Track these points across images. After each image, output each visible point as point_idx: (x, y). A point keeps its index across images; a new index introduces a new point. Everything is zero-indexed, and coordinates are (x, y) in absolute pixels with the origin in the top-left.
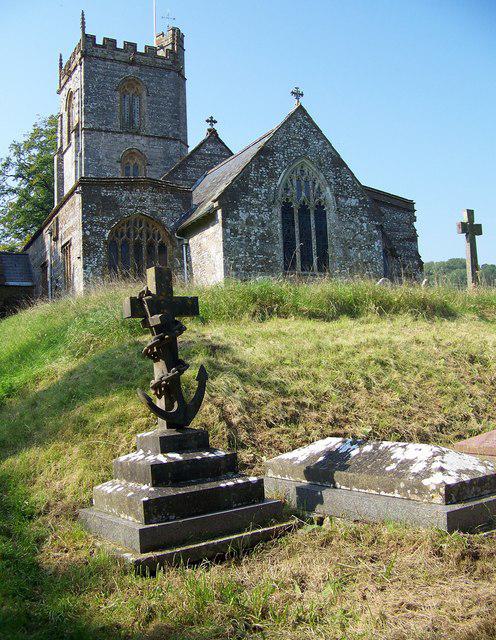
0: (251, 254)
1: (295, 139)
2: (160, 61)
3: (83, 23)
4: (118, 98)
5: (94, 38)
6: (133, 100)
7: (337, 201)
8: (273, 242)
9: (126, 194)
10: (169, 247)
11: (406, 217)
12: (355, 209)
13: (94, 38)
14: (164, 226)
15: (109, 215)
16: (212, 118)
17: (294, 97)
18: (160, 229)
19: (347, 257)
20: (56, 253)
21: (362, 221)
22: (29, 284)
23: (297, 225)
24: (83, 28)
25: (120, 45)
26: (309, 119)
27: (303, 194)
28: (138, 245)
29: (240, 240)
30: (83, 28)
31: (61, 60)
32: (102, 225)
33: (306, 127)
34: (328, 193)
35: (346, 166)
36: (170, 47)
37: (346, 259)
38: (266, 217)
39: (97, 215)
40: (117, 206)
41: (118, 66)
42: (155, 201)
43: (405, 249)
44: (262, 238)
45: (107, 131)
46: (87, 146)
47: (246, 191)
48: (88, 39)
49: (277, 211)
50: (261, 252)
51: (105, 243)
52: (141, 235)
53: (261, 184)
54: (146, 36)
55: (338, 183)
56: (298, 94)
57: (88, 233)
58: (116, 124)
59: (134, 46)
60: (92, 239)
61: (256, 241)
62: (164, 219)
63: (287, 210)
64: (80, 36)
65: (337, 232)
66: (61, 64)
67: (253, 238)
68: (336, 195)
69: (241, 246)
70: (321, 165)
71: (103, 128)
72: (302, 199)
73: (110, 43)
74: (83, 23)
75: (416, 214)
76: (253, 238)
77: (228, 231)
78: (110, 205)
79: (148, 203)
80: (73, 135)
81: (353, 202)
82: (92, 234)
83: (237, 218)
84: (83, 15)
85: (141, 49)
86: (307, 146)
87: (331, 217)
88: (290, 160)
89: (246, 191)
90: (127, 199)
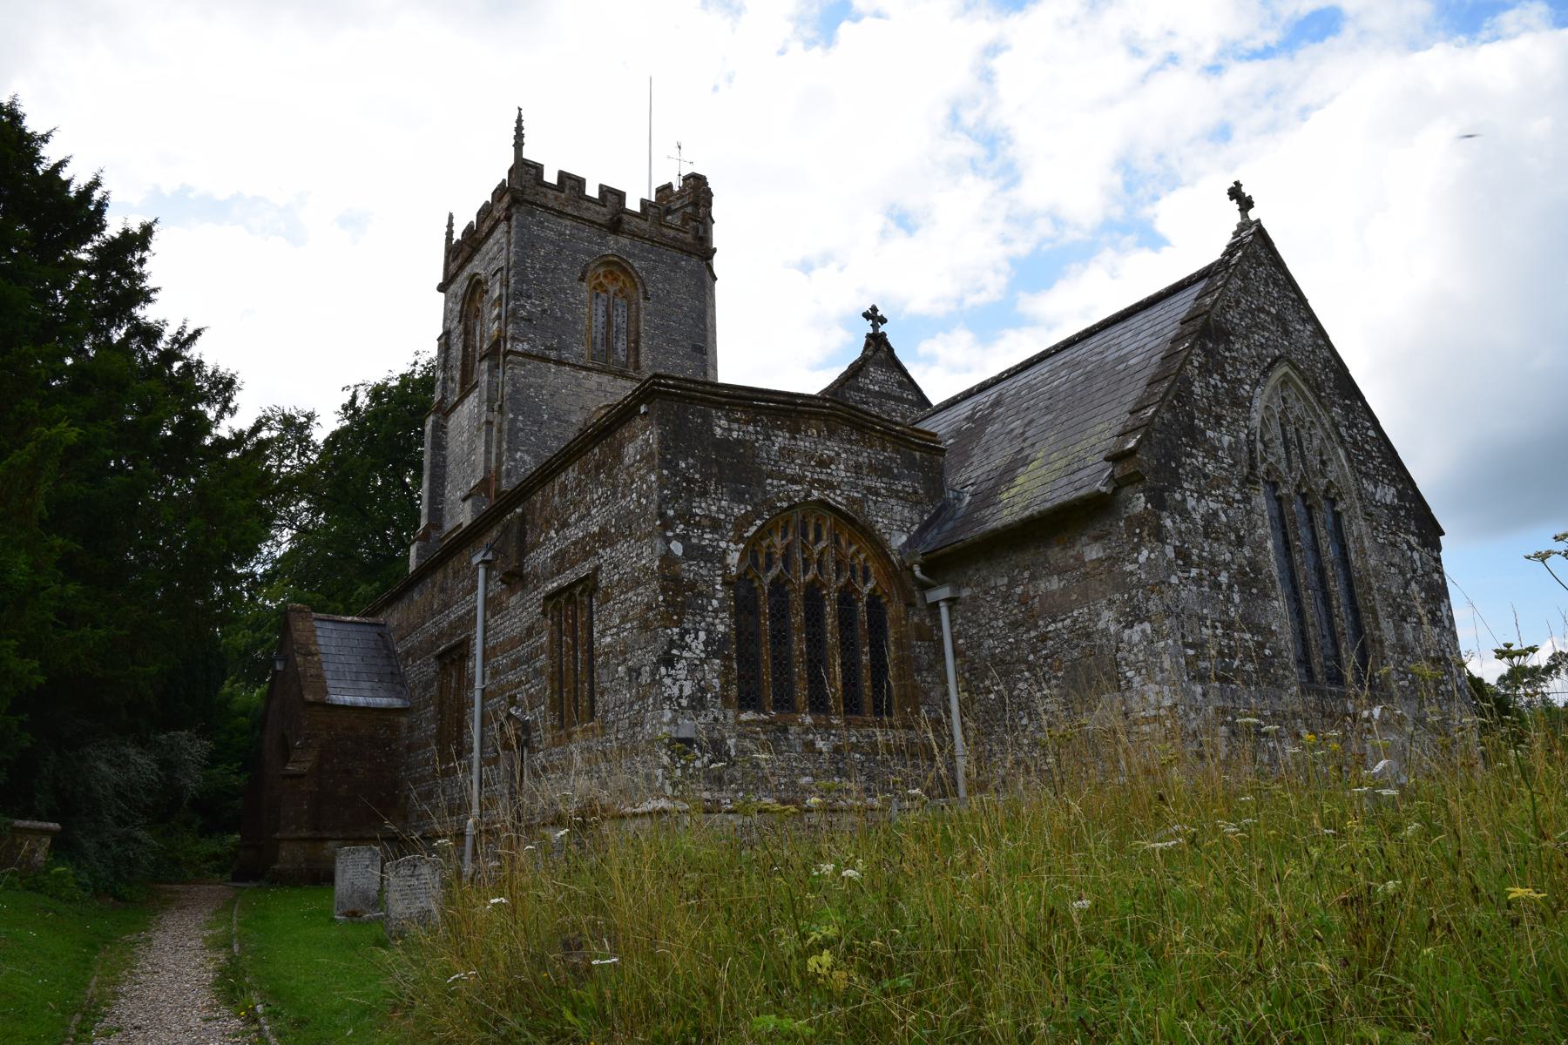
5: (538, 168)
9: (781, 439)
15: (738, 497)
16: (874, 309)
20: (853, 603)
22: (397, 703)
24: (519, 144)
30: (519, 144)
31: (450, 225)
32: (716, 526)
39: (704, 494)
41: (587, 231)
42: (858, 467)
46: (517, 391)
48: (525, 172)
57: (677, 548)
58: (579, 350)
59: (621, 196)
60: (690, 570)
64: (510, 162)
66: (450, 233)
71: (553, 354)
73: (571, 183)
79: (840, 472)
82: (693, 552)
84: (519, 121)
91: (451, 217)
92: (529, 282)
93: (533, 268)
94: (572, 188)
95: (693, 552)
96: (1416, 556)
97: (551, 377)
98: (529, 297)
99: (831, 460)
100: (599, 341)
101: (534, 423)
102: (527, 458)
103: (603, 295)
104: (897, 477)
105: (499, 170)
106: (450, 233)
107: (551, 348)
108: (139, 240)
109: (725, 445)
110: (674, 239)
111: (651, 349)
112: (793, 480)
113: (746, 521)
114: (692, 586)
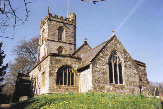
15: (57, 64)
21: (132, 69)
33: (116, 41)
34: (122, 60)
55: (125, 58)
57: (51, 69)
60: (52, 71)
87: (123, 68)
96: (133, 70)
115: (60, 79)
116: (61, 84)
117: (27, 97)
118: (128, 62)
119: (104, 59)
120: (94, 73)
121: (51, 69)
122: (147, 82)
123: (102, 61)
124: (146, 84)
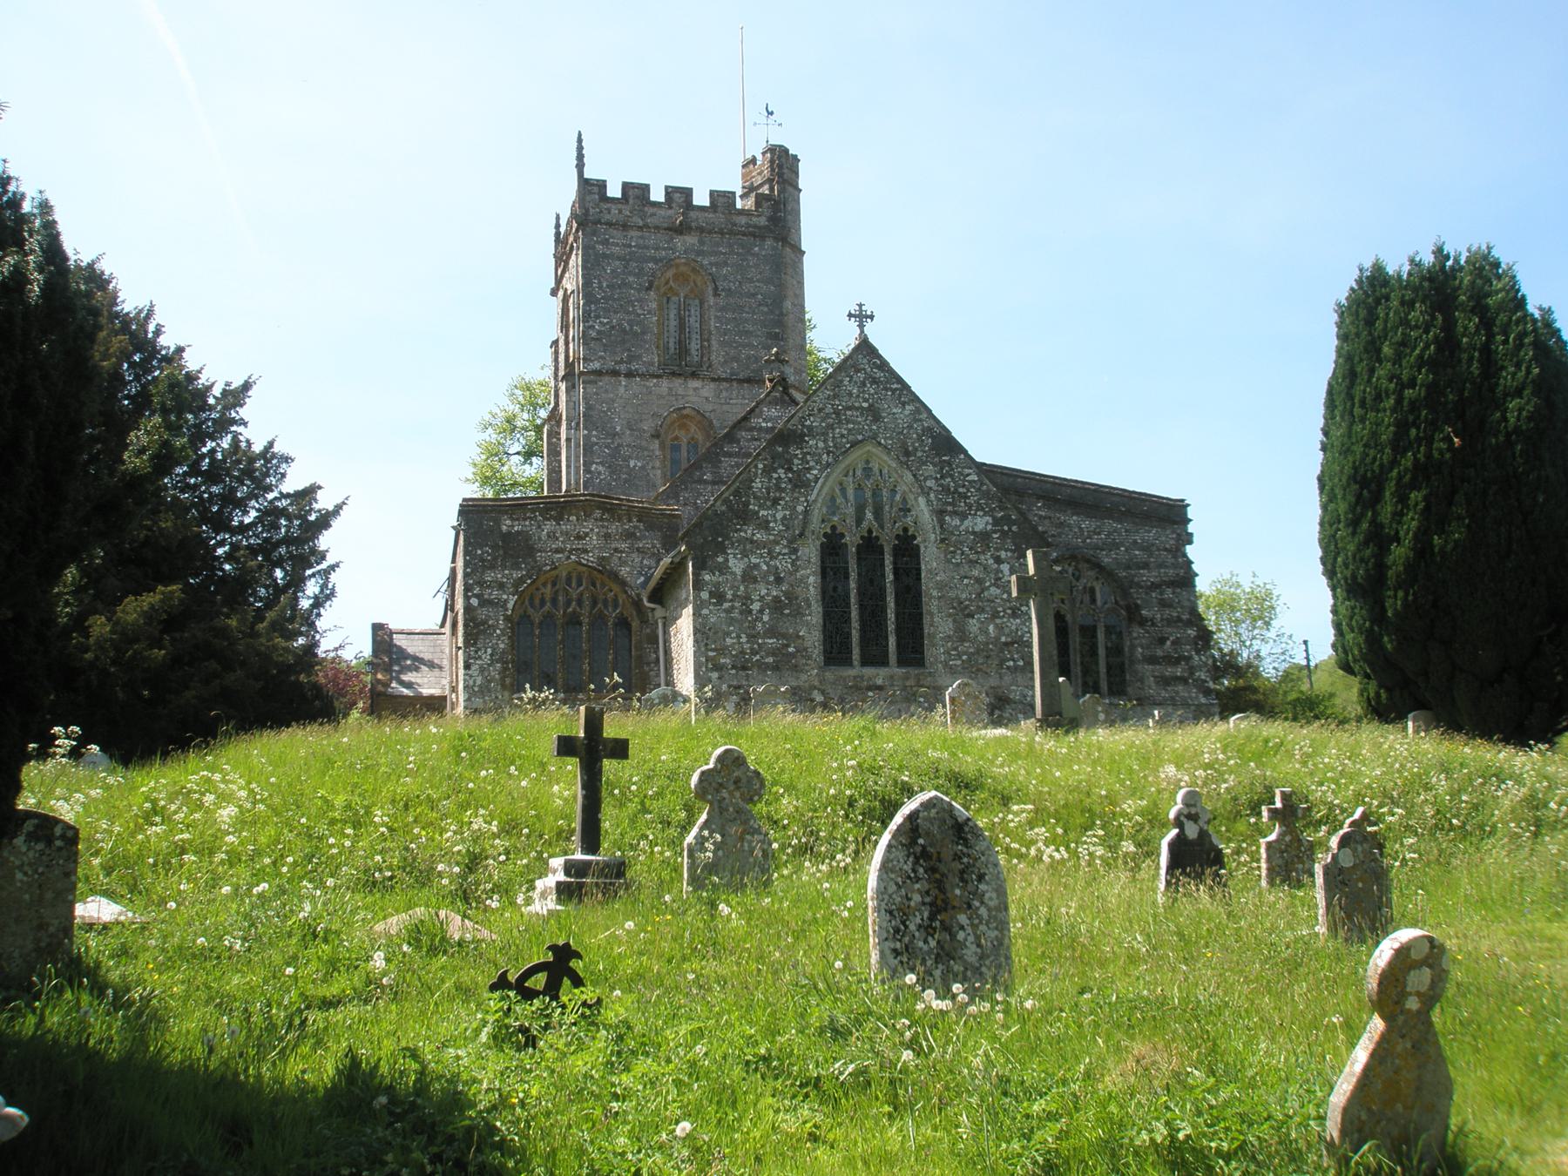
0: (752, 637)
1: (849, 408)
2: (743, 220)
3: (580, 157)
4: (654, 305)
5: (602, 185)
6: (687, 307)
7: (942, 523)
8: (798, 613)
9: (549, 526)
10: (635, 624)
11: (1168, 537)
12: (984, 536)
13: (602, 185)
14: (623, 584)
15: (516, 567)
17: (854, 324)
18: (616, 588)
19: (962, 635)
21: (998, 560)
23: (853, 575)
24: (580, 166)
25: (657, 195)
26: (884, 365)
27: (869, 515)
28: (574, 621)
29: (728, 611)
30: (580, 166)
32: (501, 586)
33: (875, 381)
34: (923, 510)
35: (965, 452)
36: (765, 190)
37: (962, 640)
38: (784, 564)
39: (492, 567)
40: (530, 551)
41: (652, 239)
42: (607, 536)
43: (1163, 604)
44: (777, 606)
45: (630, 375)
46: (589, 407)
47: (745, 516)
48: (591, 190)
49: (810, 551)
50: (772, 632)
51: (507, 619)
52: (580, 602)
53: (775, 502)
54: (713, 170)
55: (946, 490)
56: (861, 316)
57: (474, 602)
58: (652, 358)
60: (482, 614)
61: (761, 611)
62: (624, 571)
63: (832, 547)
65: (941, 586)
66: (558, 226)
67: (756, 606)
68: (940, 514)
69: (732, 621)
70: (907, 454)
71: (623, 368)
72: (865, 525)
73: (636, 193)
74: (580, 157)
75: (1191, 528)
76: (756, 606)
77: (705, 595)
78: (516, 549)
80: (563, 386)
81: (981, 523)
82: (484, 603)
83: (723, 569)
84: (580, 140)
85: (701, 199)
86: (877, 418)
87: (931, 558)
88: (838, 453)
89: (745, 516)
90: (552, 536)
91: (580, 134)
92: (597, 302)
93: (600, 287)
94: (637, 197)
95: (484, 603)
97: (622, 390)
98: (597, 317)
99: (587, 534)
100: (671, 345)
101: (608, 434)
102: (600, 468)
103: (674, 299)
104: (639, 539)
105: (564, 199)
106: (558, 226)
107: (622, 361)
108: (325, 521)
109: (508, 537)
110: (748, 226)
111: (722, 344)
112: (557, 551)
113: (521, 580)
114: (484, 622)
115: (891, 615)
116: (870, 546)
117: (606, 762)
118: (963, 516)
119: (779, 516)
120: (705, 611)
121: (474, 602)
122: (1192, 632)
123: (764, 525)
124: (1187, 650)
